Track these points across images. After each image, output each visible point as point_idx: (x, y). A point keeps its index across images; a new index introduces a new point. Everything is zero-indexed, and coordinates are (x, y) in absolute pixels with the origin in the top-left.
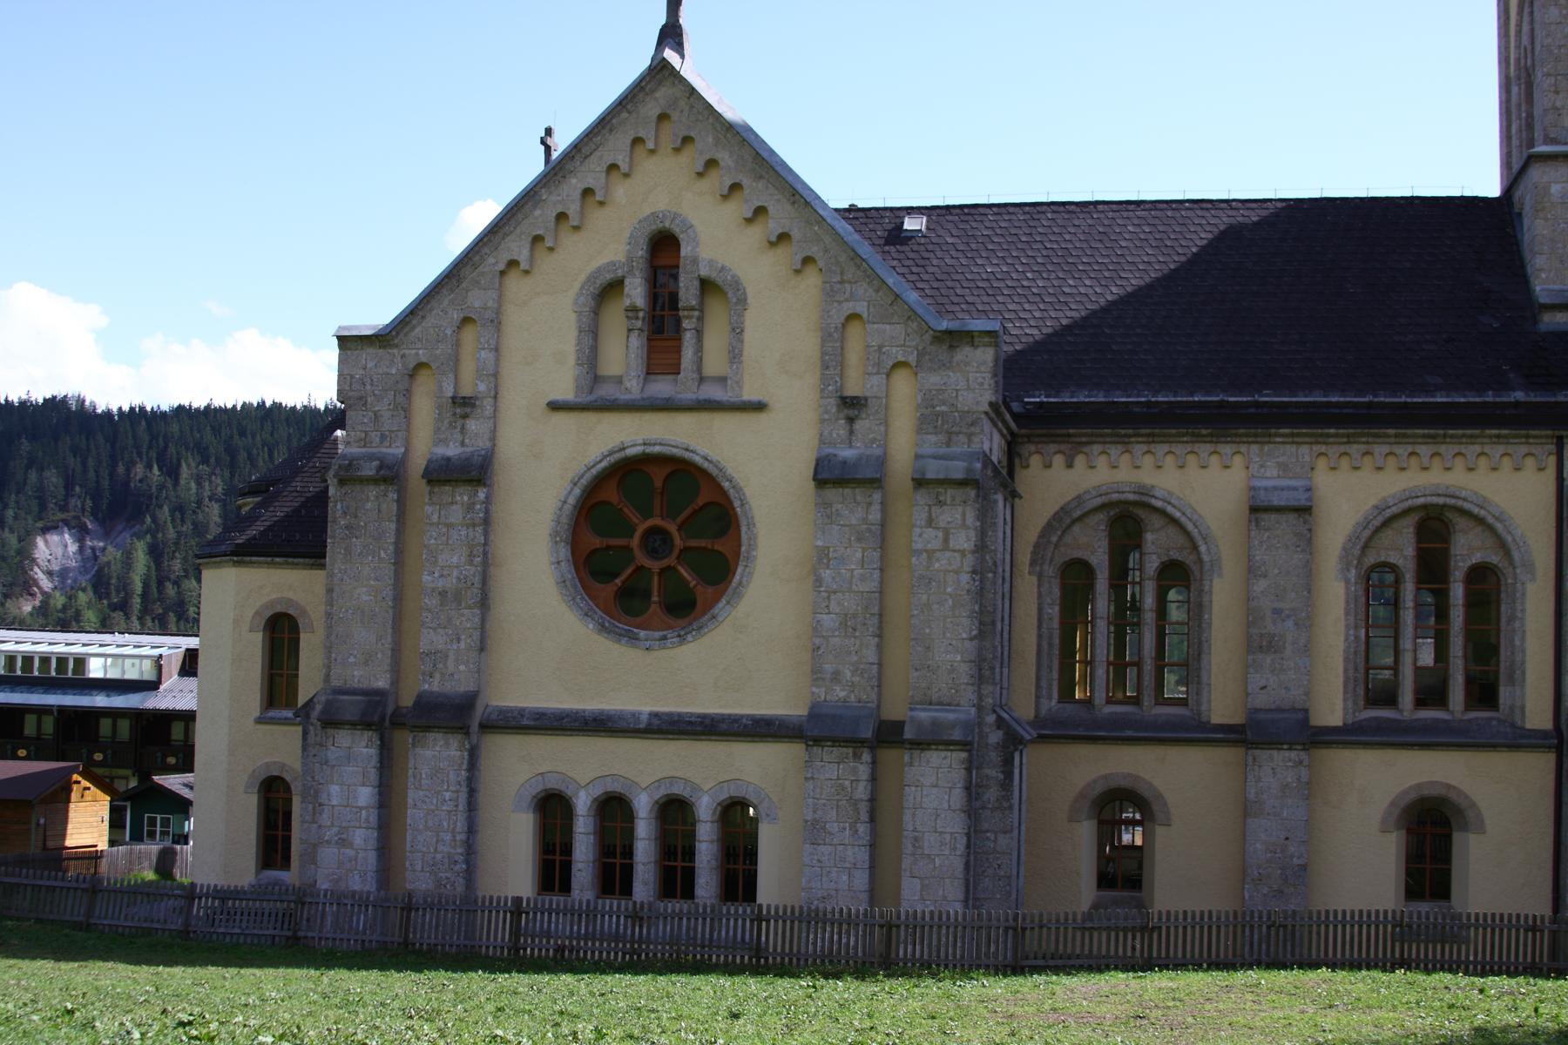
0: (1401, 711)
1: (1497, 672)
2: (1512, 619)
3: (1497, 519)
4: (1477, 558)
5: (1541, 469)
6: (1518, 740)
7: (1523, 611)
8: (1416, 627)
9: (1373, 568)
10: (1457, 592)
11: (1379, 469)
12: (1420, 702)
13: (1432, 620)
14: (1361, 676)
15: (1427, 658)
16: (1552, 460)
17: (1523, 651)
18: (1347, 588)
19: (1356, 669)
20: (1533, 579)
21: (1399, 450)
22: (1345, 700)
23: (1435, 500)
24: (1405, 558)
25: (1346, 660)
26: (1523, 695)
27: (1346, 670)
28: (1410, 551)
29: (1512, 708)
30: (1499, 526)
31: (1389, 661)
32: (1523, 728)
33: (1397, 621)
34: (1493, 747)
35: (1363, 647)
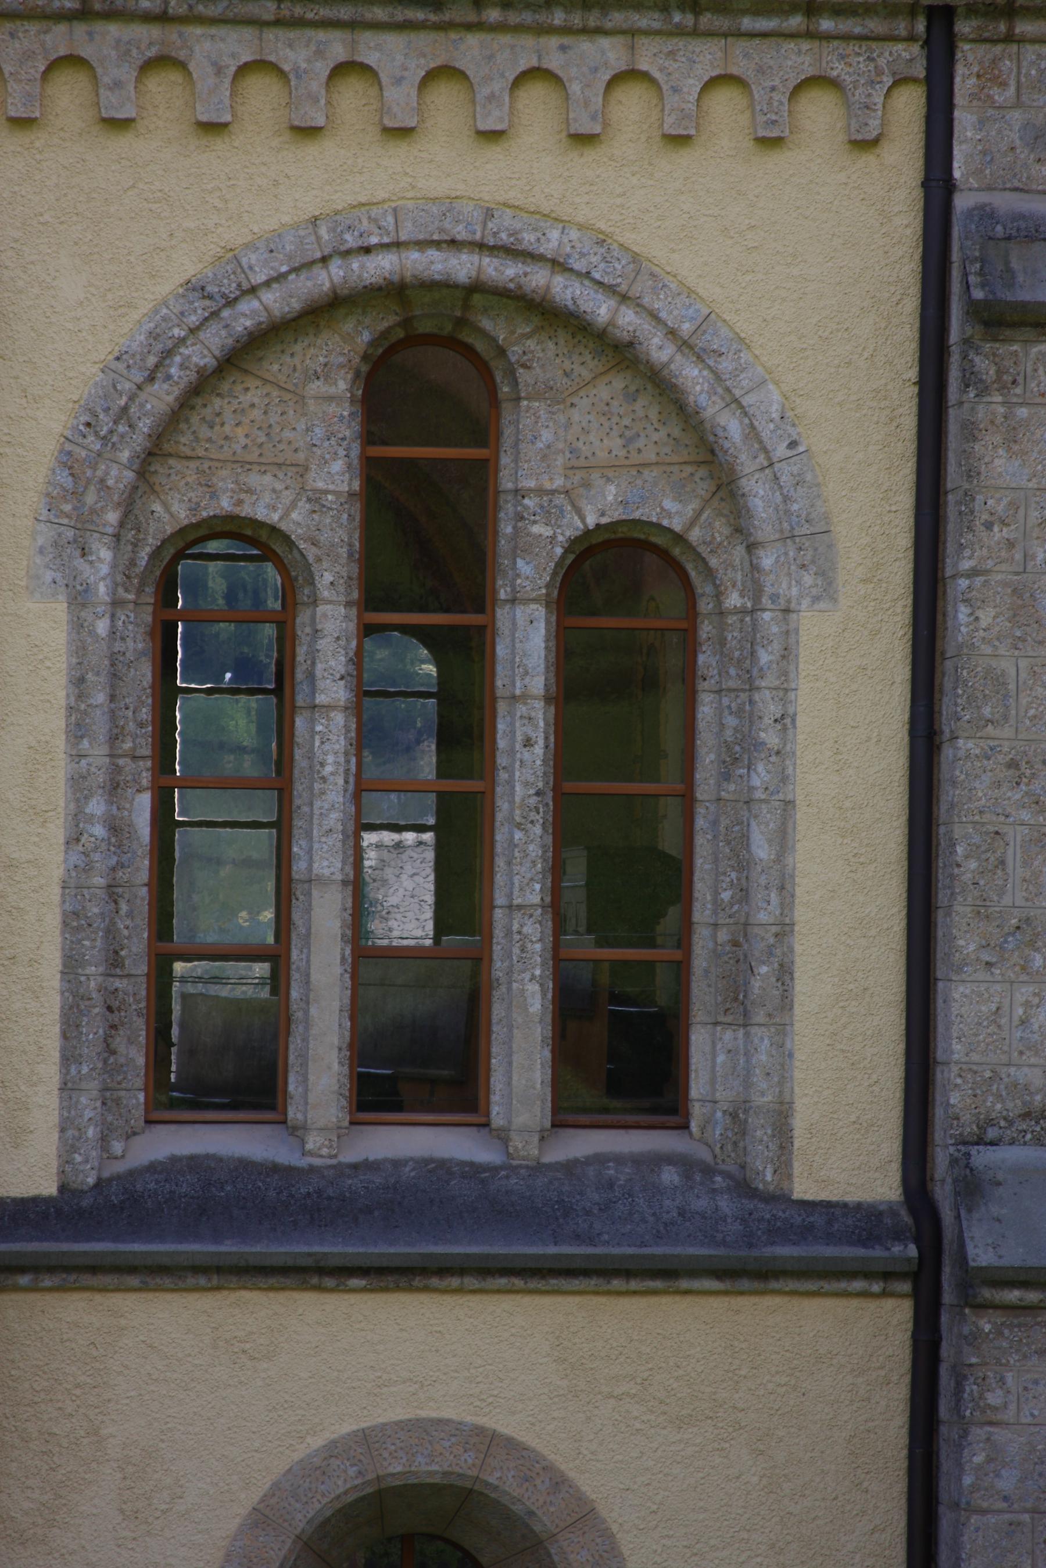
0: (297, 1132)
1: (682, 969)
2: (741, 752)
3: (685, 345)
4: (603, 505)
5: (865, 144)
6: (765, 1246)
7: (785, 721)
8: (360, 789)
9: (188, 542)
10: (525, 644)
11: (212, 128)
12: (375, 1095)
13: (426, 762)
14: (134, 989)
15: (408, 915)
16: (910, 104)
17: (785, 886)
18: (78, 625)
19: (114, 962)
20: (827, 591)
21: (293, 51)
22: (68, 1088)
23: (438, 264)
24: (316, 499)
25: (74, 922)
26: (785, 1057)
27: (71, 965)
28: (337, 474)
29: (738, 1117)
30: (691, 377)
31: (259, 922)
32: (782, 1198)
33: (284, 764)
34: (664, 1274)
35: (142, 870)
